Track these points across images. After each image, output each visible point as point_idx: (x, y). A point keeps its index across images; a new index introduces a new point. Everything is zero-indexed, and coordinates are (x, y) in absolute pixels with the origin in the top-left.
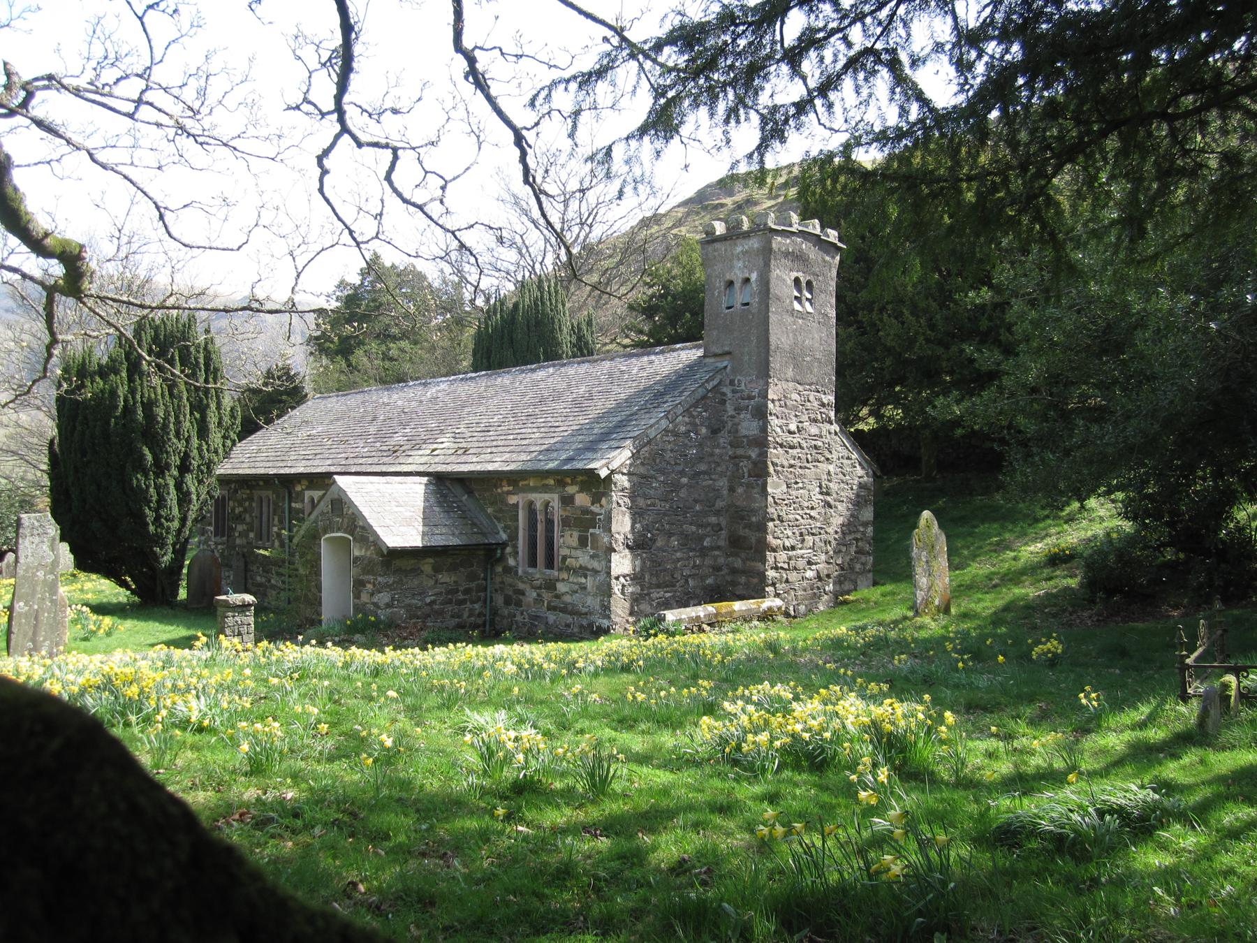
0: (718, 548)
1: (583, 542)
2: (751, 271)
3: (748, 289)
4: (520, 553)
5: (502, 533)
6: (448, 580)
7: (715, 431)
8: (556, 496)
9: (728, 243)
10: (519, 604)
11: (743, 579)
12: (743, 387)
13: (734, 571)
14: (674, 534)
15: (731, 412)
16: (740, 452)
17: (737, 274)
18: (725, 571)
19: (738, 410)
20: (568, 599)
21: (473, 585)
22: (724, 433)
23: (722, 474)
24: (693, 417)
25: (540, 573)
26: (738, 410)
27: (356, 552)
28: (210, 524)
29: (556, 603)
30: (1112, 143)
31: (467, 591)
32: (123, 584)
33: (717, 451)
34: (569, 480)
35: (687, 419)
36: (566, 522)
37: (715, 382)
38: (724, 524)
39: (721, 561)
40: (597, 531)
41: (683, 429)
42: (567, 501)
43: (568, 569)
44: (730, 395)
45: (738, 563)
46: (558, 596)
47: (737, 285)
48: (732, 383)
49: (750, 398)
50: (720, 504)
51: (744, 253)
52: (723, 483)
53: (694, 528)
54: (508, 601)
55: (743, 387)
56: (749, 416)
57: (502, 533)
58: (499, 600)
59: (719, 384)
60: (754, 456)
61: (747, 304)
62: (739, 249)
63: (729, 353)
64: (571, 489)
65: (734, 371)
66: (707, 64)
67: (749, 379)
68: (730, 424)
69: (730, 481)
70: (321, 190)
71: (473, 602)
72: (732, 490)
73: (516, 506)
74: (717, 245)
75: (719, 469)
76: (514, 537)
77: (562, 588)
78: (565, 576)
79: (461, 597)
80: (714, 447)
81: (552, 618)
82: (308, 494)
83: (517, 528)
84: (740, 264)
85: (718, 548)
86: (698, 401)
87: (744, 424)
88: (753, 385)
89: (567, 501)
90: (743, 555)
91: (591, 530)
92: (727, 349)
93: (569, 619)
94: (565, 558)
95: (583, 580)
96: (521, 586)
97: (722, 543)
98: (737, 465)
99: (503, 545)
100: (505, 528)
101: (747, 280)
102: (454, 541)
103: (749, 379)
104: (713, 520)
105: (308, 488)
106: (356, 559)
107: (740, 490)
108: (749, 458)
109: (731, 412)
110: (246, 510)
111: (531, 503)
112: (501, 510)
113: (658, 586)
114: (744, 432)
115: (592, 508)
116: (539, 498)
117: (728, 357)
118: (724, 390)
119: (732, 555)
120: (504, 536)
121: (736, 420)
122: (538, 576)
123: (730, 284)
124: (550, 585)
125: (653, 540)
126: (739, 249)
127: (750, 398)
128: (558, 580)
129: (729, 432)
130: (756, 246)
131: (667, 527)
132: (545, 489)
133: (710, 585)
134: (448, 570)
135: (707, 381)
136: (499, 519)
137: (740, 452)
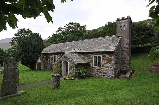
1: (107, 63)
4: (93, 64)
8: (102, 56)
17: (123, 25)
20: (104, 71)
26: (123, 44)
29: (101, 72)
30: (12, 22)
32: (28, 67)
34: (104, 53)
43: (104, 67)
46: (101, 71)
49: (125, 42)
51: (124, 22)
60: (126, 50)
63: (122, 36)
64: (105, 55)
66: (150, 1)
78: (103, 68)
81: (100, 74)
82: (54, 55)
90: (124, 64)
92: (122, 35)
94: (103, 65)
96: (93, 69)
105: (54, 54)
108: (126, 50)
111: (54, 56)
114: (124, 47)
123: (121, 26)
124: (100, 69)
136: (89, 59)
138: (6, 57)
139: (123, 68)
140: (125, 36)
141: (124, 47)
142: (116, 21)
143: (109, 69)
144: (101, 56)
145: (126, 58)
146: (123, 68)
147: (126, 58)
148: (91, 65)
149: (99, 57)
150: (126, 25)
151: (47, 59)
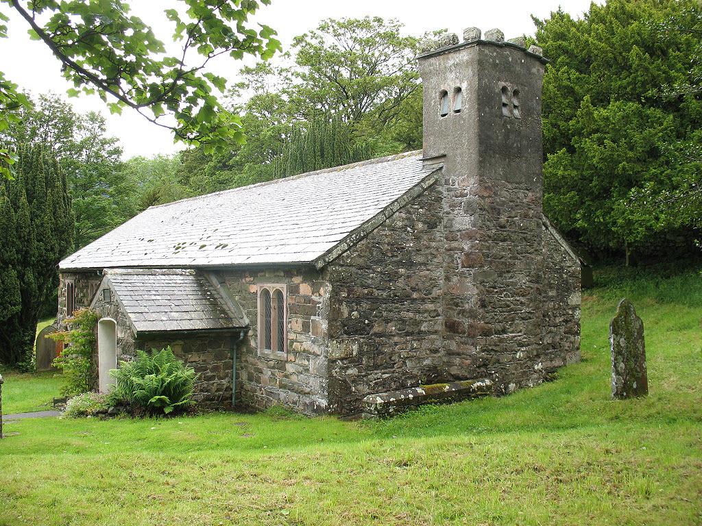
0: (436, 332)
1: (306, 327)
2: (461, 81)
3: (460, 95)
5: (245, 317)
6: (197, 359)
7: (432, 225)
8: (285, 286)
9: (442, 57)
10: (258, 381)
11: (457, 360)
12: (457, 186)
13: (450, 353)
14: (391, 320)
15: (447, 209)
16: (454, 244)
17: (450, 86)
18: (442, 352)
19: (453, 206)
20: (294, 378)
21: (220, 364)
22: (440, 227)
23: (438, 266)
24: (409, 212)
25: (275, 354)
26: (453, 206)
27: (120, 335)
28: (65, 306)
31: (215, 369)
33: (433, 244)
35: (403, 215)
36: (293, 310)
37: (431, 182)
38: (440, 310)
39: (438, 344)
40: (316, 318)
41: (400, 224)
42: (294, 290)
43: (296, 353)
44: (445, 193)
45: (453, 347)
46: (286, 376)
47: (450, 95)
48: (447, 182)
49: (463, 195)
50: (436, 292)
51: (456, 65)
52: (440, 273)
53: (411, 315)
54: (250, 379)
55: (457, 186)
56: (462, 212)
57: (245, 317)
58: (244, 376)
59: (435, 183)
60: (466, 248)
61: (458, 111)
62: (451, 62)
63: (444, 156)
64: (297, 280)
65: (448, 171)
67: (461, 178)
68: (446, 219)
69: (446, 271)
70: (203, 67)
71: (221, 378)
72: (447, 279)
73: (255, 294)
74: (432, 60)
75: (435, 260)
76: (254, 322)
77: (290, 368)
79: (210, 374)
80: (430, 240)
83: (256, 315)
84: (453, 76)
85: (436, 332)
86: (414, 199)
87: (458, 219)
88: (466, 184)
89: (294, 290)
91: (312, 317)
92: (442, 152)
93: (295, 396)
94: (292, 341)
95: (306, 363)
96: (260, 365)
97: (439, 327)
98: (452, 256)
99: (247, 327)
100: (248, 314)
101: (459, 90)
102: (198, 325)
103: (461, 178)
104: (430, 306)
106: (119, 341)
107: (455, 279)
108: (462, 250)
109: (447, 209)
110: (84, 296)
112: (244, 299)
113: (376, 367)
114: (457, 226)
115: (313, 297)
116: (272, 287)
117: (443, 160)
118: (440, 189)
119: (448, 338)
120: (246, 321)
121: (451, 216)
122: (272, 357)
123: (445, 94)
124: (281, 365)
125: (370, 325)
126: (451, 62)
127: (463, 195)
128: (287, 362)
129: (445, 227)
130: (466, 58)
131: (385, 314)
132: (278, 279)
133: (428, 366)
134: (197, 351)
135: (423, 180)
137: (454, 244)
138: (488, 388)
139: (450, 364)
140: (459, 159)
141: (457, 226)
142: (182, 146)
143: (312, 365)
144: (282, 287)
145: (467, 299)
146: (450, 364)
147: (467, 299)
148: (253, 344)
149: (279, 293)
150: (464, 86)
151: (273, 314)
